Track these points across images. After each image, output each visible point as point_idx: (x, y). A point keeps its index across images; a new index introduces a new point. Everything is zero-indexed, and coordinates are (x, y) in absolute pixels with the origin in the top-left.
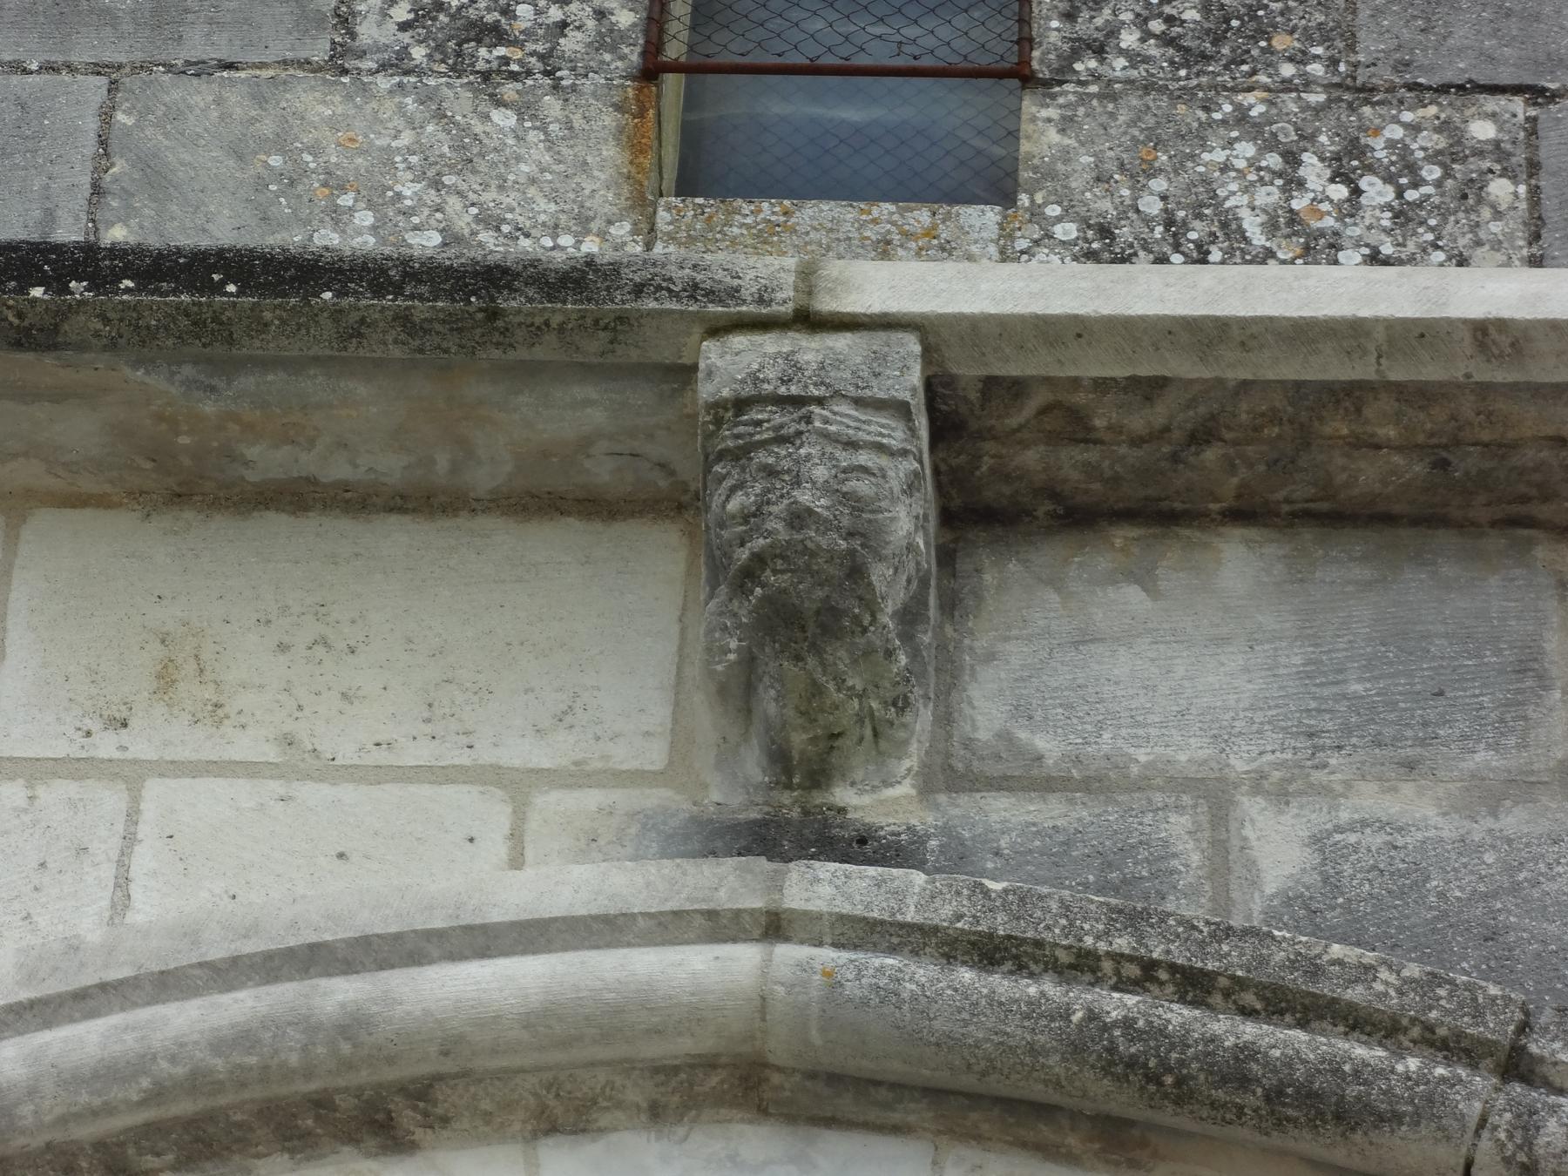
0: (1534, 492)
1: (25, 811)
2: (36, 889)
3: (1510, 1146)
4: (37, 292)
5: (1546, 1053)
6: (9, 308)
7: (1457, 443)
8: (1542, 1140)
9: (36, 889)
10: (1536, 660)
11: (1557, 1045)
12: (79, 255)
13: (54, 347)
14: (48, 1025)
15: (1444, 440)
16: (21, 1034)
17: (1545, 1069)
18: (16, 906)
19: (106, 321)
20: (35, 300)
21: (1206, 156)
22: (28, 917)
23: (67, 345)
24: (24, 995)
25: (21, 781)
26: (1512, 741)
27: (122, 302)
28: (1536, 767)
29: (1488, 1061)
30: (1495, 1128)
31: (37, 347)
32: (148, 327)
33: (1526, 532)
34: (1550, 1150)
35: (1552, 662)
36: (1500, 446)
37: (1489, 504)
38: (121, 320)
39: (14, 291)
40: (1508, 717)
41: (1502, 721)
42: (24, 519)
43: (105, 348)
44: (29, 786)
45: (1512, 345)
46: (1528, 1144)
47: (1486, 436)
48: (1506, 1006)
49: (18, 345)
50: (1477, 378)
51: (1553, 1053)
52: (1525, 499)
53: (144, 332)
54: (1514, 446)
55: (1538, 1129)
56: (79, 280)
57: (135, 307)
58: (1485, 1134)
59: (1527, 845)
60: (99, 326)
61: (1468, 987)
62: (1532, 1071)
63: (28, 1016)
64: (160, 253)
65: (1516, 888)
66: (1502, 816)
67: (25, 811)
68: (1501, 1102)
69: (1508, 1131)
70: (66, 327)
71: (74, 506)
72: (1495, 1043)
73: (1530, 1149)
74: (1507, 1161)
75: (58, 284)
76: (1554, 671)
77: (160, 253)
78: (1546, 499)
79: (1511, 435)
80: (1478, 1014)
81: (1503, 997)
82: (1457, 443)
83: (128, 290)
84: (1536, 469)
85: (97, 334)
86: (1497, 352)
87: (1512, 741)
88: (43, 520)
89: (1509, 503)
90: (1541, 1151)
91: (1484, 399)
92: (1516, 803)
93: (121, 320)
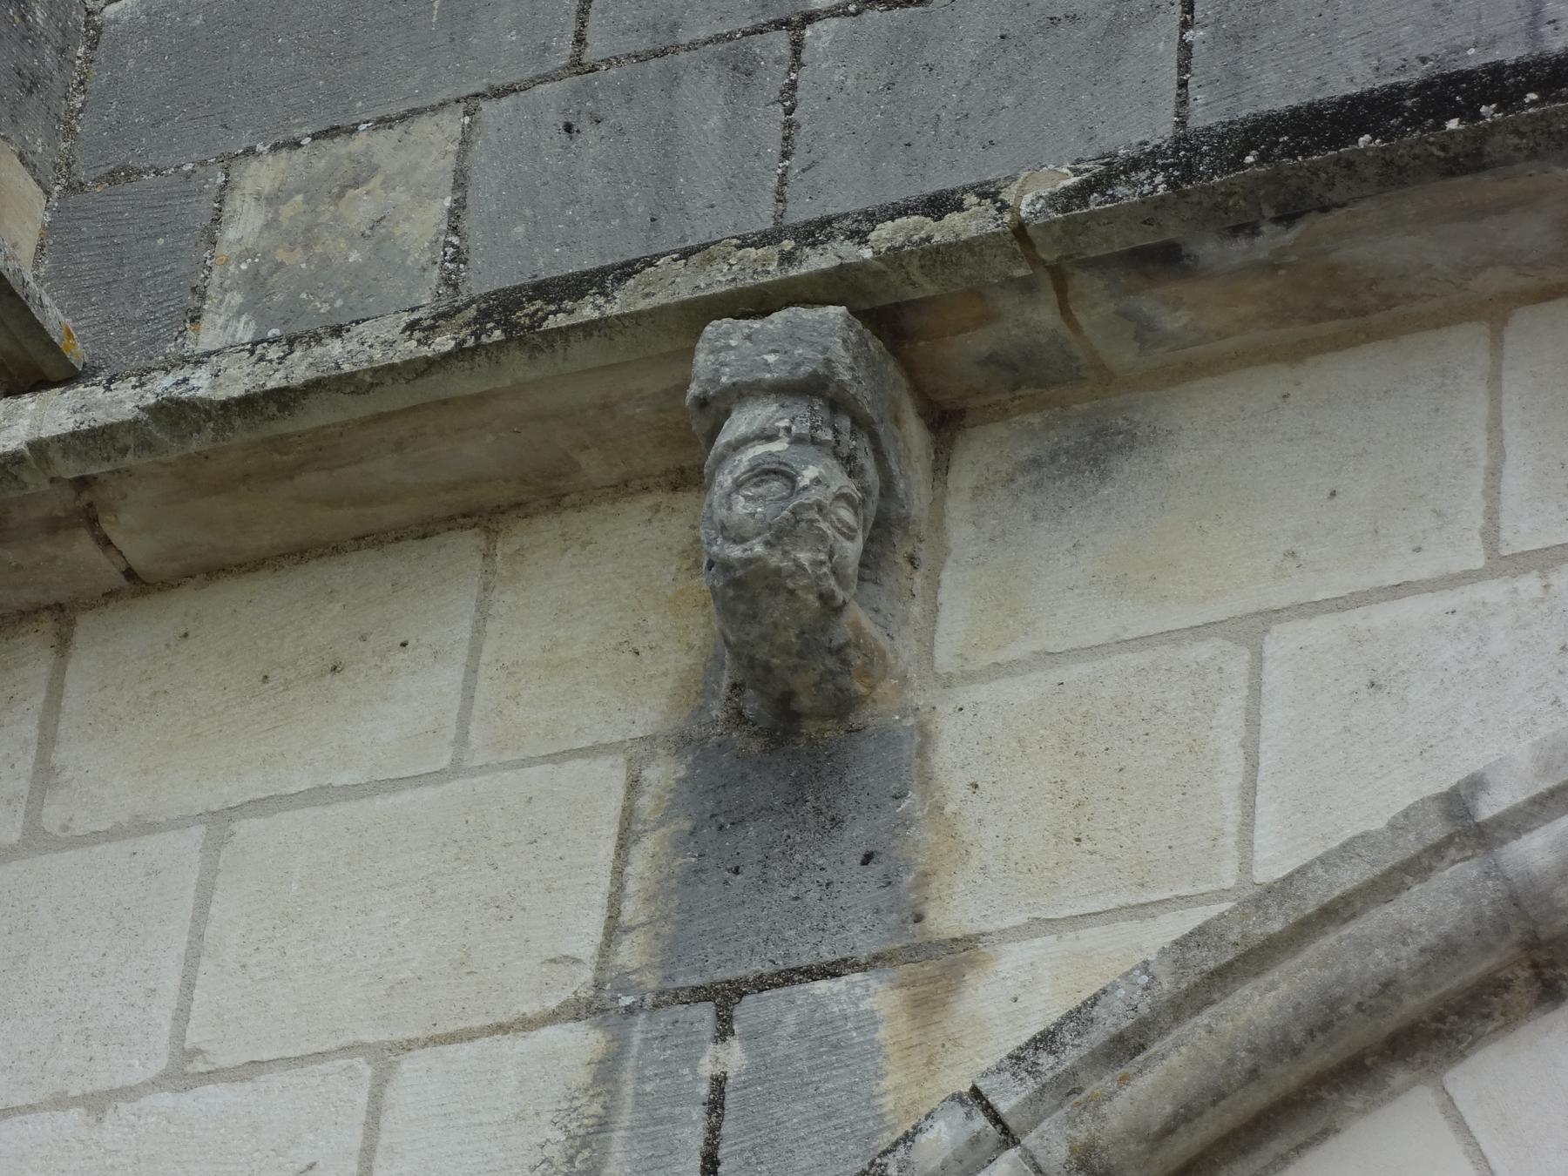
1: (1542, 600)
2: (1561, 673)
4: (1453, 124)
6: (1432, 144)
9: (1561, 673)
12: (1487, 79)
13: (1483, 168)
14: (1325, 1018)
16: (1548, 822)
18: (1545, 692)
19: (1522, 135)
20: (1452, 132)
21: (886, 1084)
22: (1556, 701)
23: (1494, 164)
24: (1544, 786)
25: (1535, 573)
27: (1529, 116)
31: (1466, 171)
32: (1560, 132)
38: (1534, 131)
39: (1433, 128)
42: (1505, 321)
43: (1528, 158)
44: (1543, 576)
49: (1450, 174)
53: (1558, 137)
56: (1488, 104)
57: (1543, 117)
60: (1516, 141)
63: (1551, 804)
64: (1558, 60)
67: (1542, 600)
70: (1488, 149)
71: (1548, 299)
75: (1469, 113)
77: (1558, 60)
83: (1533, 103)
85: (1517, 148)
88: (1523, 318)
93: (1534, 131)
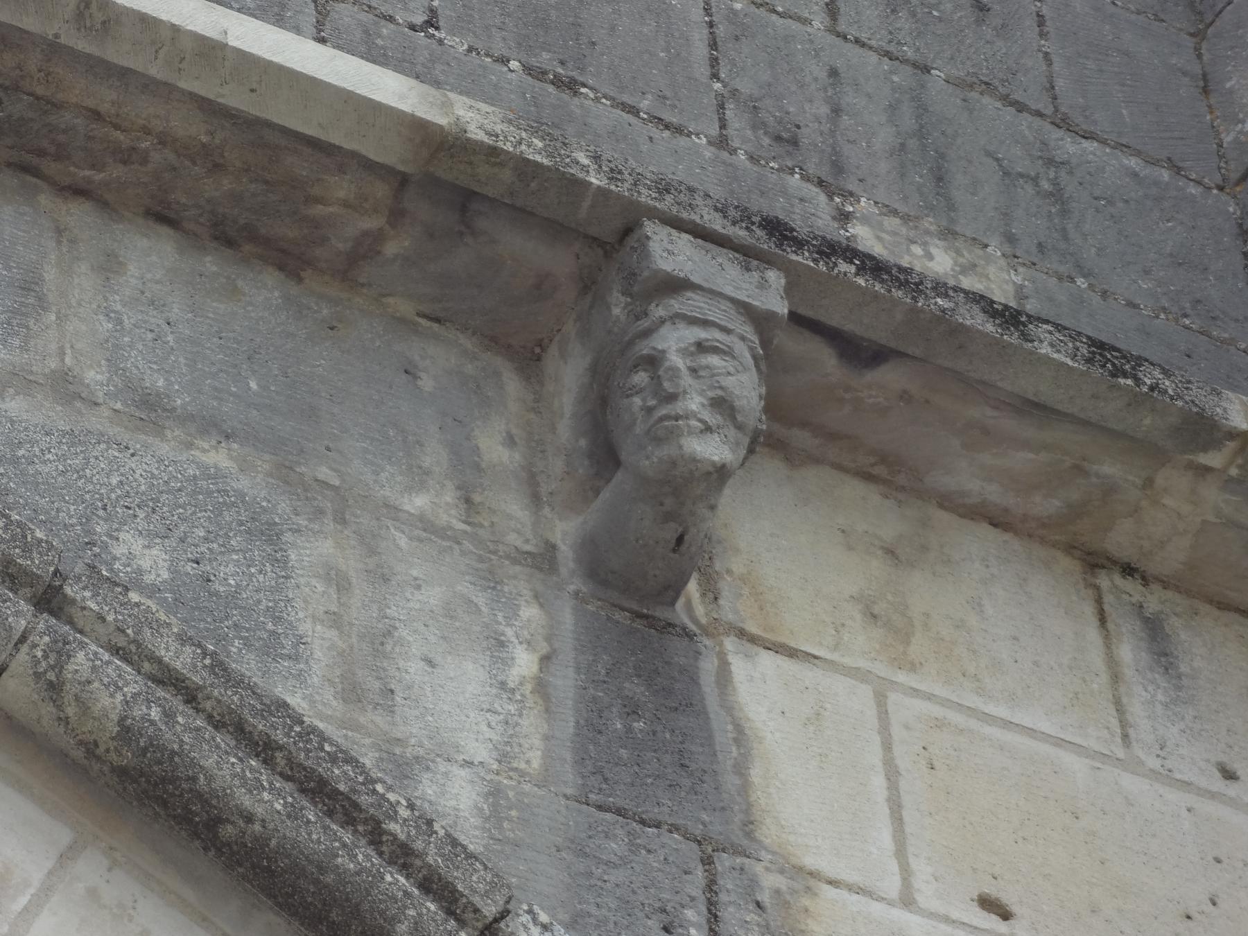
0: (52, 149)
3: (44, 664)
5: (78, 598)
7: (17, 88)
8: (71, 667)
10: (37, 284)
11: (87, 594)
15: (7, 83)
17: (73, 611)
26: (17, 342)
28: (34, 368)
29: (28, 590)
30: (35, 646)
33: (34, 180)
34: (77, 677)
35: (48, 290)
36: (48, 102)
37: (12, 148)
40: (15, 322)
41: (9, 324)
45: (104, 23)
46: (59, 667)
47: (40, 91)
48: (49, 550)
50: (63, 40)
51: (84, 599)
52: (41, 153)
54: (59, 106)
55: (69, 657)
58: (25, 648)
59: (26, 429)
61: (19, 524)
62: (61, 609)
65: (15, 461)
66: (7, 400)
68: (41, 626)
69: (45, 651)
72: (39, 577)
73: (61, 672)
74: (37, 676)
76: (51, 298)
78: (58, 158)
79: (60, 96)
80: (27, 550)
81: (47, 542)
82: (17, 88)
84: (65, 131)
86: (88, 25)
87: (17, 342)
89: (28, 152)
90: (69, 676)
91: (49, 60)
92: (18, 394)
